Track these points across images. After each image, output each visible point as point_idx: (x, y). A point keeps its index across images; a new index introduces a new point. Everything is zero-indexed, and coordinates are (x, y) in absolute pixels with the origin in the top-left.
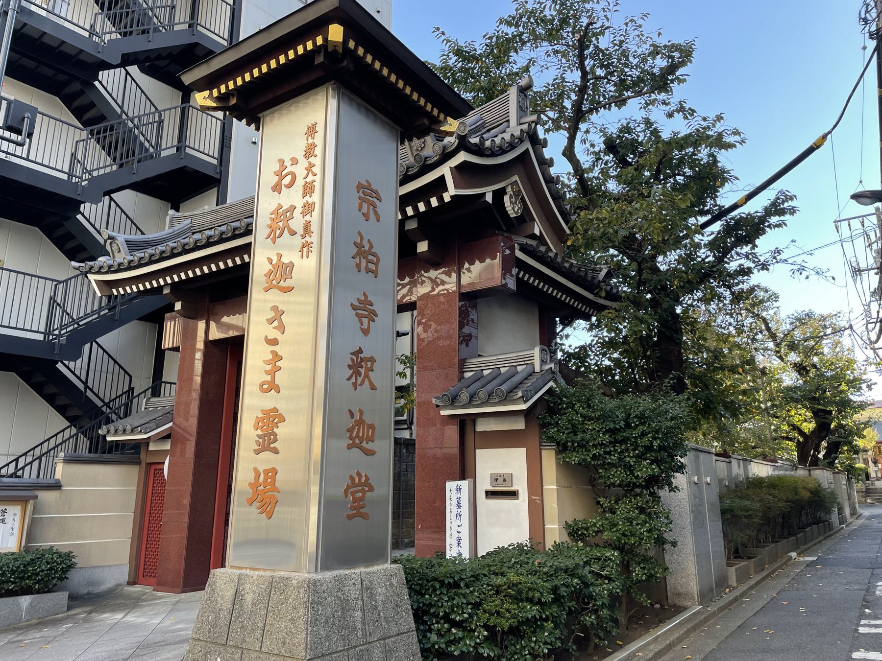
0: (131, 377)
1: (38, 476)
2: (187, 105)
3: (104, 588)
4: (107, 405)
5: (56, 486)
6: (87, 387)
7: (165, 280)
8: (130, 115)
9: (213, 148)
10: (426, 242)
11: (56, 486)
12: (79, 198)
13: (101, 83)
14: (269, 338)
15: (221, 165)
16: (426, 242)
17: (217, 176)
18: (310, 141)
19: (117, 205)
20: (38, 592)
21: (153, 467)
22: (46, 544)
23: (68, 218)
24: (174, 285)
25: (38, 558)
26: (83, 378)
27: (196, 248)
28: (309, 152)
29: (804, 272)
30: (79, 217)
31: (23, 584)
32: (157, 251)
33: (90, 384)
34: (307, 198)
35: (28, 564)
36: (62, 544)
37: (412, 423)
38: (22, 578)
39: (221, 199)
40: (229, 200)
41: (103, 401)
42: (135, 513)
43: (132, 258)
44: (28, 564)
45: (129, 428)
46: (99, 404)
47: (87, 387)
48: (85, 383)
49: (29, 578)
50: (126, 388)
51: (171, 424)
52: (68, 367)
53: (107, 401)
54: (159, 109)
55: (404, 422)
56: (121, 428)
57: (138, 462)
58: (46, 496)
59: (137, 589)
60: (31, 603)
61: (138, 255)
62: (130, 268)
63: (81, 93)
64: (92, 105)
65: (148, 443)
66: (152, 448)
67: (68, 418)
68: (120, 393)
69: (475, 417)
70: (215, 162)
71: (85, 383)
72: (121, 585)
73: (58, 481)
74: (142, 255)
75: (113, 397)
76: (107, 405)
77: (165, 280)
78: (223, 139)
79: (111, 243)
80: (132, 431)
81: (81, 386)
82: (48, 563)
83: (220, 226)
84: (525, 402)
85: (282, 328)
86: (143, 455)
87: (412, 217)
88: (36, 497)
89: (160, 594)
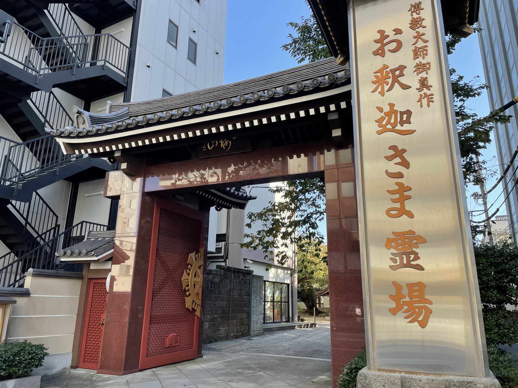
0: (57, 217)
1: (4, 286)
2: (99, 35)
3: (55, 371)
4: (40, 236)
5: (27, 294)
6: (27, 222)
7: (117, 147)
8: (66, 35)
9: (123, 64)
10: (340, 129)
11: (27, 294)
12: (36, 86)
13: (49, 11)
14: (389, 171)
15: (128, 78)
16: (340, 129)
17: (125, 85)
18: (415, 16)
19: (54, 96)
20: (19, 377)
21: (93, 282)
22: (21, 338)
23: (20, 101)
24: (124, 150)
25: (22, 350)
26: (25, 216)
27: (159, 123)
28: (415, 24)
29: (494, 176)
30: (29, 101)
31: (11, 370)
32: (104, 128)
33: (29, 220)
34: (420, 59)
35: (15, 355)
36: (33, 338)
37: (227, 258)
38: (10, 366)
39: (127, 99)
40: (132, 100)
41: (37, 233)
42: (78, 315)
43: (91, 129)
44: (15, 355)
45: (84, 251)
46: (35, 235)
47: (27, 222)
48: (26, 220)
49: (16, 366)
50: (53, 226)
51: (112, 250)
52: (14, 207)
53: (40, 233)
54: (85, 34)
55: (222, 257)
56: (77, 251)
57: (81, 278)
58: (21, 301)
59: (80, 372)
60: (15, 386)
61: (106, 126)
62: (87, 136)
63: (34, 16)
64: (41, 25)
65: (90, 264)
66: (92, 267)
67: (9, 245)
68: (49, 228)
69: (89, 263)
70: (124, 75)
71: (26, 220)
72: (66, 368)
73: (28, 290)
74: (100, 127)
75: (44, 231)
76: (40, 236)
77: (117, 147)
78: (130, 61)
79: (77, 117)
80: (87, 255)
81: (23, 222)
82: (29, 354)
83: (171, 110)
84: (97, 256)
85: (405, 164)
86: (85, 273)
87: (333, 111)
88: (15, 302)
89: (106, 376)
